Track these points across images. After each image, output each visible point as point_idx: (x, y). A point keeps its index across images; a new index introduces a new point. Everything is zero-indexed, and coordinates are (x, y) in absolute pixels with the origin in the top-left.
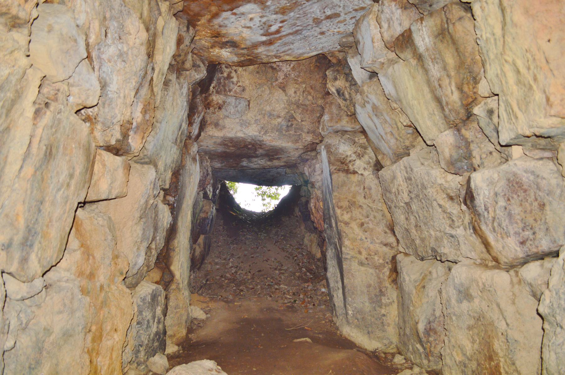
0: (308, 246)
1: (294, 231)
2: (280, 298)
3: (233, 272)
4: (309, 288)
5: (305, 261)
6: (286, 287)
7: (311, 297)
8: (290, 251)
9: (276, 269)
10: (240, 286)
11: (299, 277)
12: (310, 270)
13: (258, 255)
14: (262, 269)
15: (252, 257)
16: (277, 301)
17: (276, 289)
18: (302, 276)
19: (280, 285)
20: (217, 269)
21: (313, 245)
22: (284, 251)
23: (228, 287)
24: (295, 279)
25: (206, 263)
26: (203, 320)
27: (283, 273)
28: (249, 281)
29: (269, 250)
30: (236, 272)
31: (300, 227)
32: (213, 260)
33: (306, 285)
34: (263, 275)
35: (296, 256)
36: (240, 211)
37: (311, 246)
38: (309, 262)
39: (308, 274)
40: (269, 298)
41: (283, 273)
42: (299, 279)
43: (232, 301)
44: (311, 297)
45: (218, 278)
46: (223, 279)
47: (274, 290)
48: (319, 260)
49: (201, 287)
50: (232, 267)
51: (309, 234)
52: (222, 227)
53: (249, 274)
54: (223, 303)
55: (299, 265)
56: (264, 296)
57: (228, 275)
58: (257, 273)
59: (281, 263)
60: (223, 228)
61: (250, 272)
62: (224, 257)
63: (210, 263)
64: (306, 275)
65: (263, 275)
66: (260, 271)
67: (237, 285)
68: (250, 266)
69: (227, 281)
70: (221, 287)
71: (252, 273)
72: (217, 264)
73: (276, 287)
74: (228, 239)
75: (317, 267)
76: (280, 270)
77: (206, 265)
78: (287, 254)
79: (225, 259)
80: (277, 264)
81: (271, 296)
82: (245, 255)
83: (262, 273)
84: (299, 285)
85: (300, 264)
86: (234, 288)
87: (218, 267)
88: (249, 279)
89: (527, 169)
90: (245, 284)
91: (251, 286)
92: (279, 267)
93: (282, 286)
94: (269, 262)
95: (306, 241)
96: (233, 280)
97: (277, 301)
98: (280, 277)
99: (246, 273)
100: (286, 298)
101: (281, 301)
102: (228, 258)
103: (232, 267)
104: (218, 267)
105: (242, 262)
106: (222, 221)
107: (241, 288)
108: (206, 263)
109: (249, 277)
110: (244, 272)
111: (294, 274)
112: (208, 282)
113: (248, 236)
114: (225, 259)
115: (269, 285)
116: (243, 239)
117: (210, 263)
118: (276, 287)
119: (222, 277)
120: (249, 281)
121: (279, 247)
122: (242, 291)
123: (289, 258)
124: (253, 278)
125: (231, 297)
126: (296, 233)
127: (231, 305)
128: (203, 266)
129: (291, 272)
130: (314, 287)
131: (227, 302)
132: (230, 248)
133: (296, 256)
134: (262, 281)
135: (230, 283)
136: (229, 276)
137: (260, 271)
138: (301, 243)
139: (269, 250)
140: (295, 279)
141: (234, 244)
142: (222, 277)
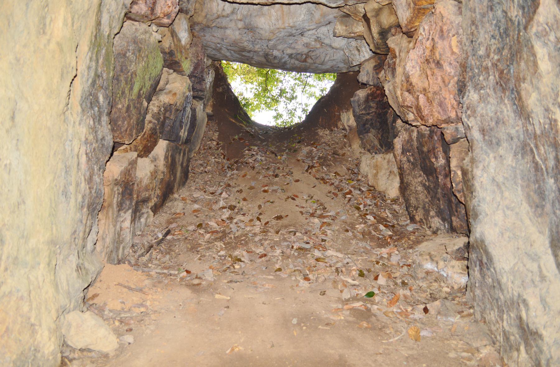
0: (370, 176)
1: (341, 152)
2: (329, 284)
3: (224, 217)
4: (395, 259)
5: (368, 202)
6: (340, 255)
7: (403, 283)
8: (337, 183)
9: (312, 215)
10: (235, 248)
11: (363, 233)
12: (381, 220)
13: (275, 187)
14: (283, 214)
15: (265, 191)
16: (323, 293)
17: (318, 260)
18: (370, 233)
19: (325, 249)
20: (195, 211)
21: (381, 174)
22: (325, 183)
23: (209, 248)
24: (355, 236)
25: (176, 199)
26: (106, 356)
27: (329, 225)
28: (257, 239)
29: (297, 181)
30: (231, 218)
31: (350, 146)
32: (191, 195)
33: (384, 251)
34: (286, 227)
35: (350, 192)
36: (248, 122)
37: (376, 175)
38: (376, 205)
39: (381, 227)
40: (304, 284)
41: (329, 225)
42: (364, 239)
43: (212, 288)
44: (403, 283)
45: (191, 228)
46: (202, 231)
47: (312, 262)
48: (395, 201)
49: (151, 247)
50: (224, 208)
51: (369, 155)
52: (215, 143)
53: (258, 223)
54: (186, 293)
55: (358, 209)
56: (290, 276)
57: (213, 224)
58: (274, 222)
59: (322, 204)
60: (218, 144)
61: (259, 219)
62: (211, 190)
63: (184, 199)
64: (376, 229)
65: (286, 227)
66: (279, 218)
67: (230, 246)
68: (260, 207)
69: (208, 236)
70: (194, 248)
71: (263, 222)
72: (195, 201)
73: (317, 253)
74: (225, 161)
75: (395, 215)
76: (321, 217)
77: (176, 203)
78: (332, 189)
79: (212, 193)
80: (315, 206)
81: (306, 279)
82: (251, 188)
83: (284, 221)
84: (367, 252)
85: (361, 207)
86: (222, 253)
87: (196, 206)
88: (255, 234)
89: (107, 305)
90: (247, 243)
91: (260, 250)
92: (319, 212)
93: (330, 253)
94: (298, 201)
95: (365, 168)
96: (223, 236)
97: (323, 293)
98: (324, 233)
99: (251, 220)
100: (345, 284)
101: (333, 293)
102: (219, 191)
103: (224, 208)
104: (196, 206)
105: (245, 199)
106: (217, 134)
107: (237, 253)
108: (176, 199)
109: (257, 230)
110: (246, 219)
111: (353, 226)
112: (169, 237)
113: (259, 157)
114: (212, 193)
115: (300, 249)
116: (250, 160)
117: (184, 199)
118: (317, 253)
119: (200, 226)
120: (257, 239)
121: (314, 176)
122: (240, 260)
123: (336, 195)
124: (264, 232)
125: (209, 276)
126: (344, 155)
127: (205, 298)
128: (169, 204)
129: (345, 222)
130: (405, 257)
131: (195, 288)
132: (226, 176)
133: (350, 192)
134: (285, 240)
135: (216, 239)
136: (215, 225)
137: (279, 218)
138: (356, 171)
139: (297, 181)
140: (355, 236)
141: (233, 170)
142: (200, 226)
